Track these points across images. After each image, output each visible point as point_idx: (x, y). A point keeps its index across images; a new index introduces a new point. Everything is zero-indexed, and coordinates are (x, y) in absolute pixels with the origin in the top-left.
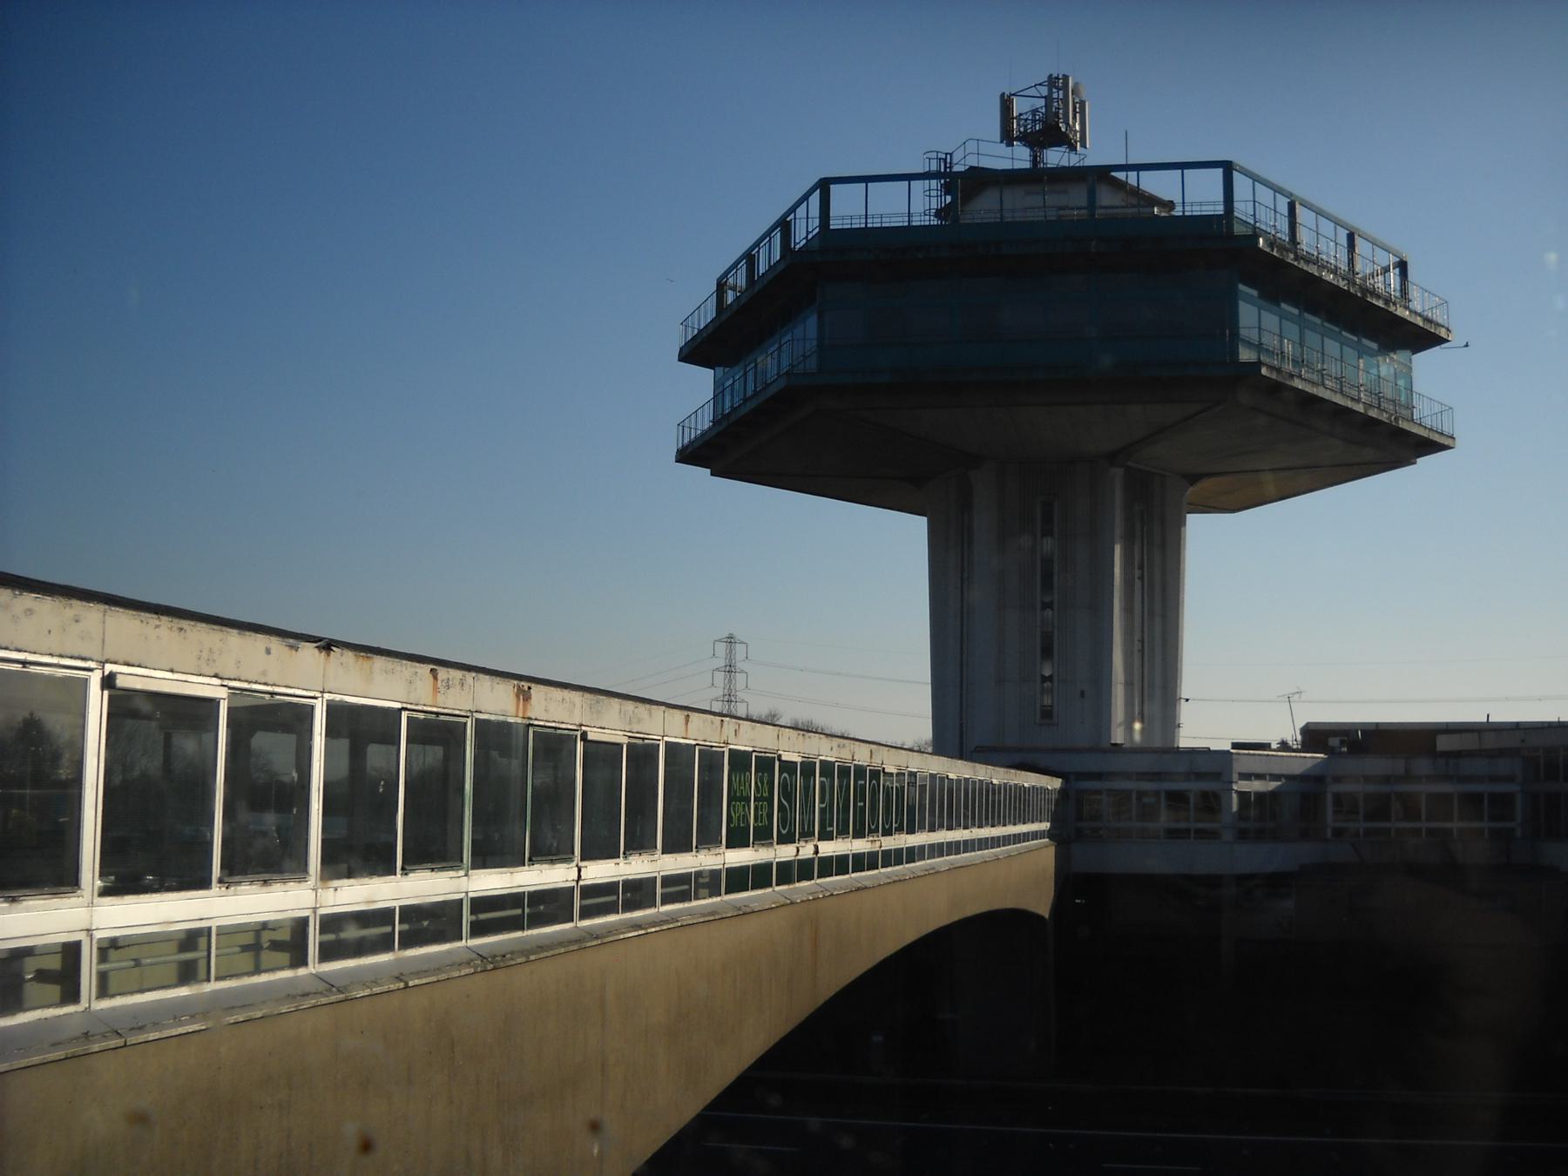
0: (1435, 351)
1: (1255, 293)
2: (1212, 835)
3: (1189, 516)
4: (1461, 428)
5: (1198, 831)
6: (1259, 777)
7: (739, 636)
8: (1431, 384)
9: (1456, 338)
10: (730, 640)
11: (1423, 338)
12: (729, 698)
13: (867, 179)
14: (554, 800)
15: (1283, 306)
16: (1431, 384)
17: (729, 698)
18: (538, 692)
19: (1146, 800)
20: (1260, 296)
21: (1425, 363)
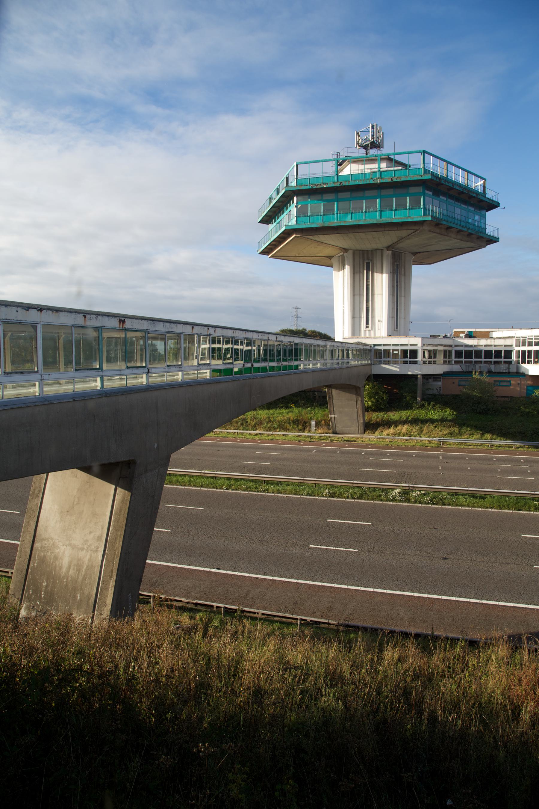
0: (494, 211)
1: (431, 193)
2: (416, 362)
3: (413, 266)
4: (500, 234)
5: (410, 361)
6: (441, 345)
7: (298, 307)
8: (493, 221)
9: (501, 206)
10: (296, 308)
11: (493, 205)
12: (193, 328)
13: (322, 161)
14: (285, 355)
15: (441, 197)
16: (493, 221)
17: (193, 328)
18: (195, 327)
19: (395, 352)
20: (433, 194)
21: (490, 215)
